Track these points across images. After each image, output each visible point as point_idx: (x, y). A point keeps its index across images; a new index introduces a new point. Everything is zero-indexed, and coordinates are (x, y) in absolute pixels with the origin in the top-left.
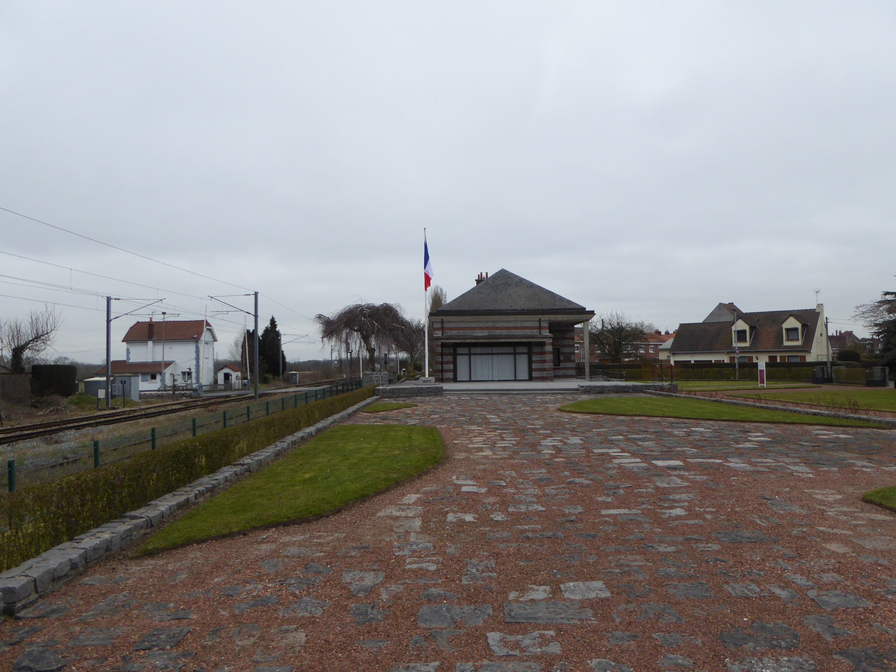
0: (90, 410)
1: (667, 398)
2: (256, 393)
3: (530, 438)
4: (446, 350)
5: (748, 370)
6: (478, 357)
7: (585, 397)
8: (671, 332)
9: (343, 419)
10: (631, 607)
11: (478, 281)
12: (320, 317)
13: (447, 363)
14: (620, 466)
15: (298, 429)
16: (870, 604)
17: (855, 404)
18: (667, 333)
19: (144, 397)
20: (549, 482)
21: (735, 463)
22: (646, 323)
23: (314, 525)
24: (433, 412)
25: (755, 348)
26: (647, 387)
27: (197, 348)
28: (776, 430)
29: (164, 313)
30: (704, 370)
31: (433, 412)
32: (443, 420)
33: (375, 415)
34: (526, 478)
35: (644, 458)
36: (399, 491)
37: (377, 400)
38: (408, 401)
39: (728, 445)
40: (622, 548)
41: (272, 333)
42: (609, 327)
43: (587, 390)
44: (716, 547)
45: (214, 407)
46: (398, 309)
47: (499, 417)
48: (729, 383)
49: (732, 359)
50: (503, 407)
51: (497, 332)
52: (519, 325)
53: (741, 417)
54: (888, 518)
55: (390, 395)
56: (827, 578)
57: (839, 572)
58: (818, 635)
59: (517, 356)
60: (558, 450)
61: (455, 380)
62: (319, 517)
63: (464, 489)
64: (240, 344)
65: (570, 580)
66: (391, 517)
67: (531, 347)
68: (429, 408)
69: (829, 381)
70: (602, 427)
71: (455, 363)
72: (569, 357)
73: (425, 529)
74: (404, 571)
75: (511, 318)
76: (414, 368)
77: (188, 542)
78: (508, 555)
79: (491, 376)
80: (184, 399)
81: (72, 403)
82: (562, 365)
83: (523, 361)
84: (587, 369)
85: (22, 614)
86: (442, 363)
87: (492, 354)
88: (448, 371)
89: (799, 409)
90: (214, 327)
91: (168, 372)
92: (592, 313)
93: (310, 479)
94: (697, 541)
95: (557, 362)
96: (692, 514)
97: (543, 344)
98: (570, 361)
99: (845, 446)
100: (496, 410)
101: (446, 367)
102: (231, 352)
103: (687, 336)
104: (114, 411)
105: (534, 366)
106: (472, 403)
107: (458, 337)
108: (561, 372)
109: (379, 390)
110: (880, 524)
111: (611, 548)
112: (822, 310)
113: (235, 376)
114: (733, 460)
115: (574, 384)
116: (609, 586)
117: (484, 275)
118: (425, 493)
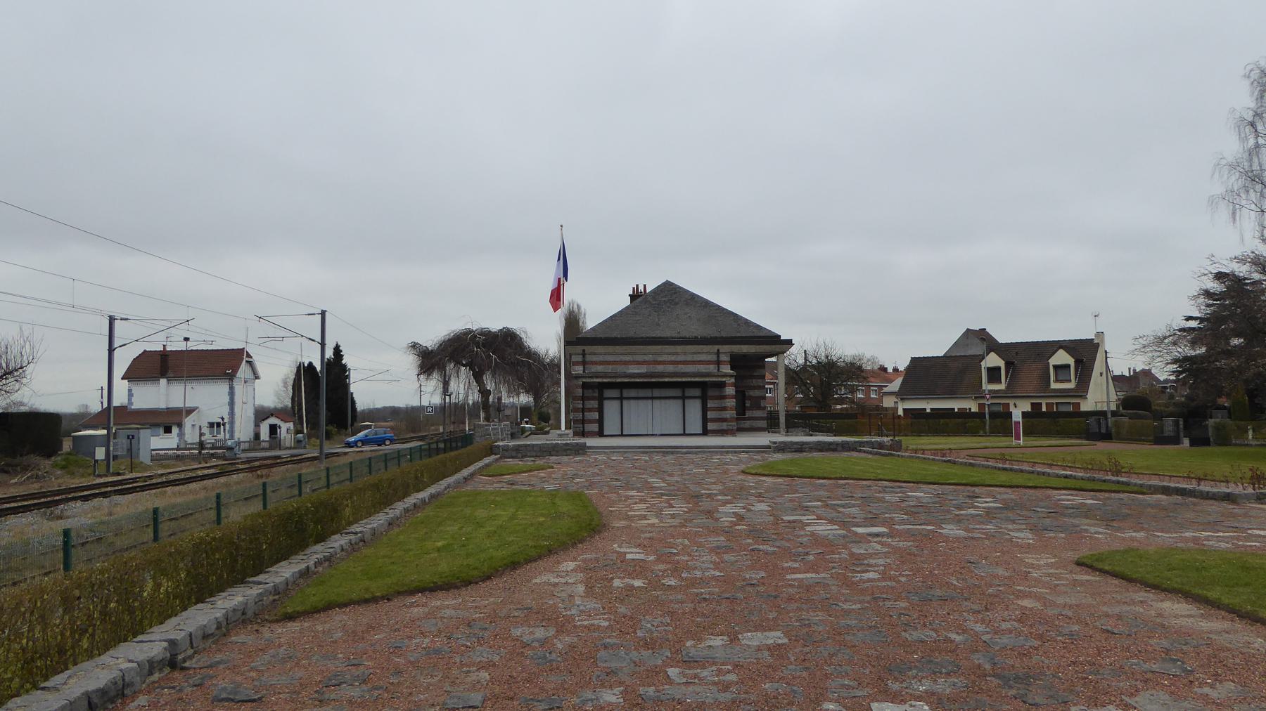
0: (83, 476)
1: (884, 458)
2: (321, 453)
3: (706, 504)
4: (589, 393)
5: (1000, 422)
6: (632, 402)
7: (778, 457)
8: (901, 368)
9: (458, 484)
10: (808, 649)
11: (634, 297)
12: (414, 346)
13: (590, 410)
14: (813, 534)
15: (406, 495)
16: (1036, 643)
17: (1116, 464)
18: (896, 370)
19: (159, 458)
20: (728, 550)
21: (950, 530)
22: (868, 355)
23: (463, 591)
24: (575, 476)
25: (1011, 392)
26: (861, 444)
27: (232, 388)
28: (1010, 495)
29: (186, 339)
30: (942, 421)
31: (575, 476)
32: (591, 485)
33: (498, 478)
34: (700, 545)
35: (843, 524)
36: (553, 558)
37: (497, 460)
38: (540, 462)
39: (948, 511)
40: (805, 607)
41: (336, 368)
42: (814, 361)
43: (781, 448)
44: (903, 604)
45: (265, 472)
46: (523, 336)
47: (664, 480)
48: (975, 439)
49: (981, 406)
50: (668, 469)
51: (660, 368)
52: (689, 358)
53: (971, 480)
54: (1088, 578)
55: (514, 454)
56: (1004, 626)
57: (1019, 621)
58: (979, 666)
59: (687, 401)
60: (740, 518)
61: (601, 434)
62: (467, 583)
63: (629, 556)
64: (291, 383)
65: (749, 631)
66: (549, 584)
67: (706, 389)
68: (570, 470)
69: (1107, 437)
70: (797, 491)
71: (601, 410)
72: (757, 403)
73: (590, 592)
74: (575, 626)
75: (679, 349)
76: (542, 417)
77: (328, 607)
78: (684, 613)
79: (650, 426)
80: (214, 462)
81: (55, 465)
82: (749, 414)
83: (694, 408)
84: (782, 419)
85: (187, 665)
86: (583, 410)
87: (652, 398)
88: (591, 422)
89: (1048, 470)
90: (256, 359)
91: (188, 422)
92: (789, 343)
93: (444, 547)
94: (884, 599)
95: (741, 410)
96: (884, 576)
97: (722, 385)
98: (760, 408)
99: (1086, 512)
100: (659, 473)
101: (589, 415)
102: (277, 395)
103: (923, 374)
104: (120, 478)
105: (710, 415)
106: (628, 464)
107: (605, 375)
108: (747, 424)
109: (498, 447)
110: (1082, 583)
111: (794, 606)
112: (1103, 340)
113: (285, 428)
114: (948, 527)
115: (763, 439)
116: (787, 634)
117: (641, 288)
118: (584, 561)
